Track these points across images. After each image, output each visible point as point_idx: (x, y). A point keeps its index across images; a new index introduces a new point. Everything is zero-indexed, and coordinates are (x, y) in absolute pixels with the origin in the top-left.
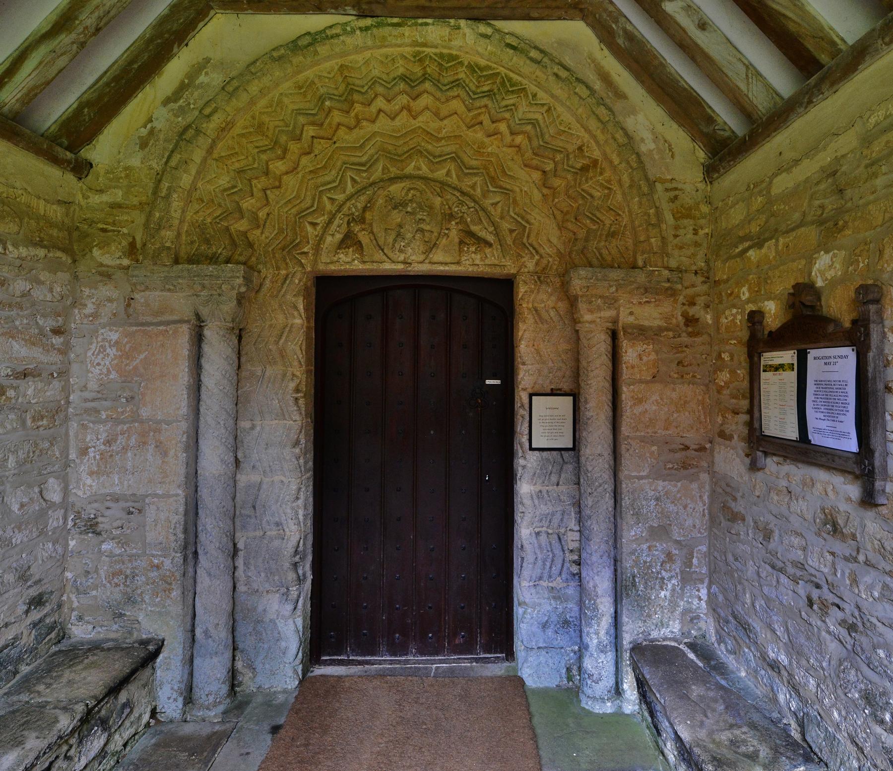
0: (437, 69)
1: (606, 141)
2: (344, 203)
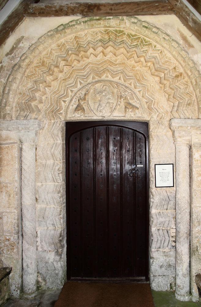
1: (185, 66)
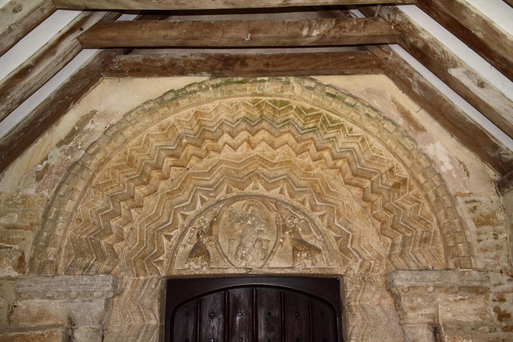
0: (272, 112)
1: (412, 165)
2: (195, 218)
